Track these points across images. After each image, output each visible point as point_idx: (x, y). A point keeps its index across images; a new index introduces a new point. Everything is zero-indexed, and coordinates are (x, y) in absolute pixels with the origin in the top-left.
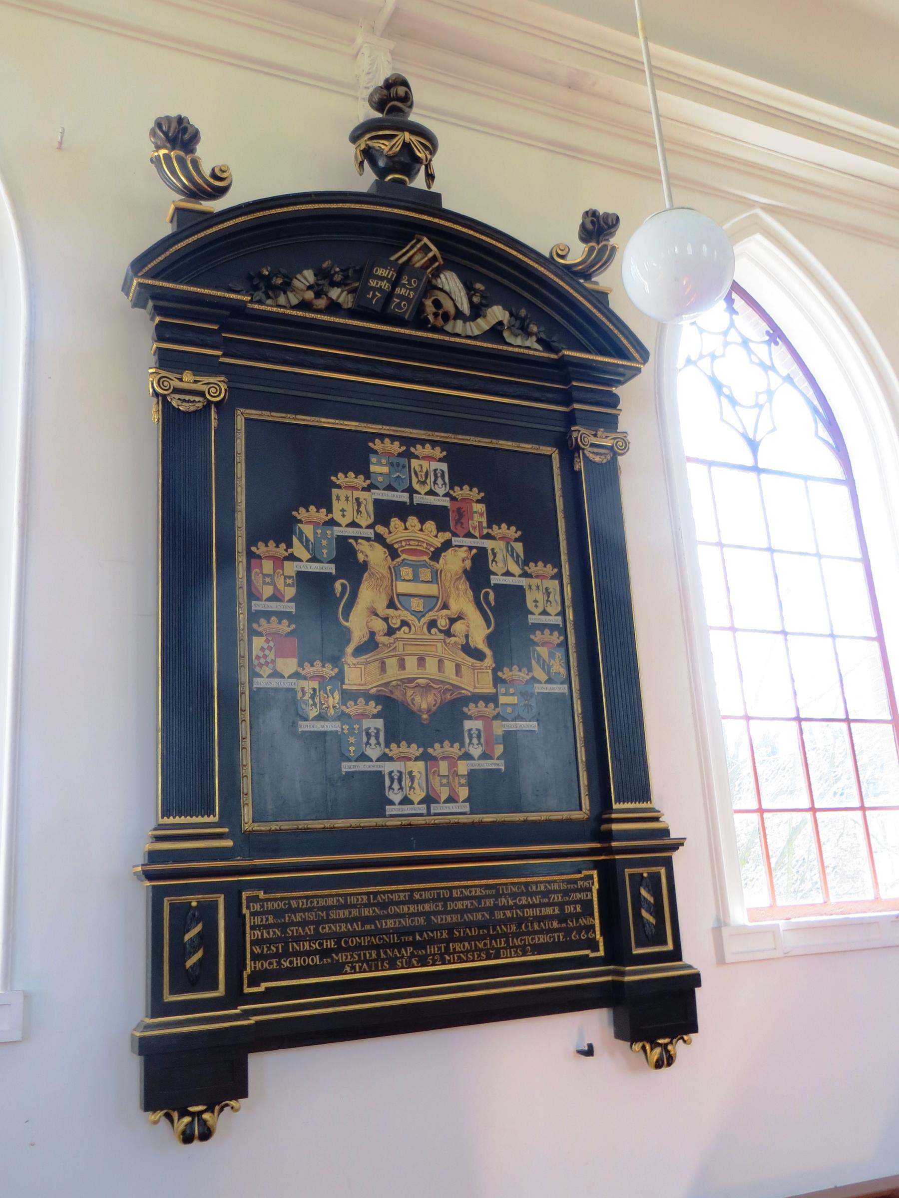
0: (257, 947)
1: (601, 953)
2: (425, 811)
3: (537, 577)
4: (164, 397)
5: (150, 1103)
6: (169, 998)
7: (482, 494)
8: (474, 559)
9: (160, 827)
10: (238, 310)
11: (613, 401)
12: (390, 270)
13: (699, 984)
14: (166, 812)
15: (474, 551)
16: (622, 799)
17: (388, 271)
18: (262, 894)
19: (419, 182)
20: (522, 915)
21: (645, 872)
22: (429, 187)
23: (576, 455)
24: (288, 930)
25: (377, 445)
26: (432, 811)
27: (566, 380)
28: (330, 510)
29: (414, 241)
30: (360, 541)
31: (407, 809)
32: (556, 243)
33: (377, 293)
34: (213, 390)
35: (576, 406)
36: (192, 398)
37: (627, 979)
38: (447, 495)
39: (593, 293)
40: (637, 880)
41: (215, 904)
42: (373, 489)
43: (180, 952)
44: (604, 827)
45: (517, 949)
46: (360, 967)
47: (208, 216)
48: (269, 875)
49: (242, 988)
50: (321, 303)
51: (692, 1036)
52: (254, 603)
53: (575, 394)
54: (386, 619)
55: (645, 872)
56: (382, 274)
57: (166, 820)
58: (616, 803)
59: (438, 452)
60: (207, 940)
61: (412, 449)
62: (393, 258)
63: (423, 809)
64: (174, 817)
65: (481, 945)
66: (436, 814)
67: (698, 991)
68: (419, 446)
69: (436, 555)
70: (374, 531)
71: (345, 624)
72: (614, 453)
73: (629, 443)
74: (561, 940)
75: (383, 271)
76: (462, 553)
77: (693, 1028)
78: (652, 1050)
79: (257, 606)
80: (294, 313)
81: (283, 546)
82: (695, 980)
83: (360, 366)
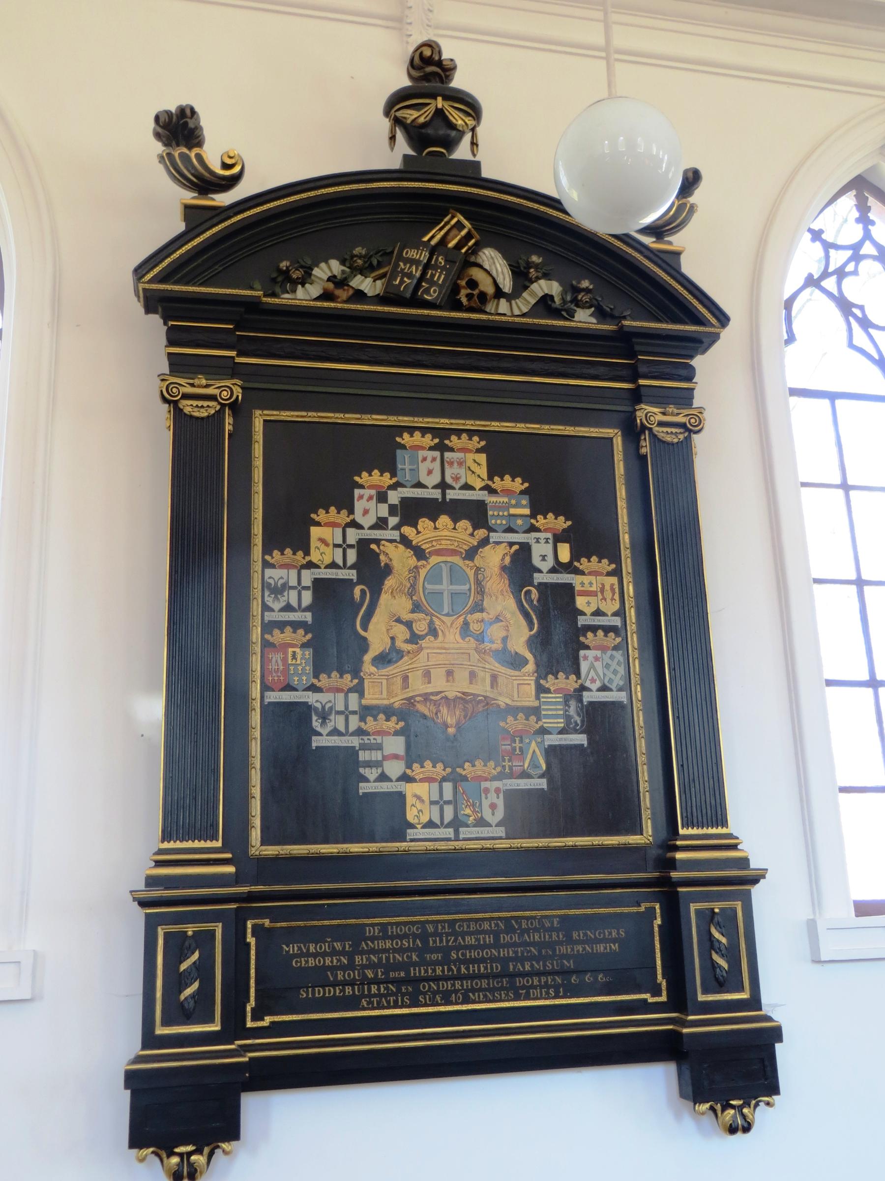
0: (369, 971)
1: (664, 998)
2: (452, 836)
3: (590, 573)
4: (176, 403)
5: (137, 1140)
6: (160, 1031)
7: (526, 485)
8: (515, 557)
9: (161, 852)
10: (253, 306)
11: (689, 375)
12: (423, 250)
13: (780, 1039)
14: (166, 836)
15: (516, 547)
16: (710, 823)
17: (420, 251)
18: (268, 922)
19: (462, 152)
20: (590, 951)
21: (717, 907)
22: (474, 155)
23: (643, 438)
24: (452, 954)
25: (406, 439)
26: (461, 836)
27: (632, 355)
28: (351, 511)
29: (450, 215)
30: (383, 542)
31: (485, 832)
32: (224, 151)
33: (405, 279)
34: (225, 393)
35: (642, 382)
36: (205, 403)
37: (685, 1031)
38: (486, 488)
39: (659, 254)
40: (709, 917)
41: (212, 933)
42: (400, 487)
43: (176, 981)
44: (669, 855)
45: (508, 992)
46: (378, 1003)
47: (218, 211)
48: (192, 907)
49: (245, 1023)
50: (343, 294)
51: (775, 1097)
52: (266, 613)
53: (642, 369)
54: (409, 624)
55: (717, 907)
56: (413, 255)
57: (166, 845)
58: (683, 829)
59: (476, 442)
60: (204, 970)
61: (447, 442)
62: (426, 239)
63: (449, 832)
64: (175, 842)
65: (536, 982)
66: (465, 840)
67: (778, 1046)
68: (454, 438)
69: (471, 554)
70: (400, 533)
71: (362, 633)
72: (690, 430)
73: (704, 420)
74: (337, 994)
75: (414, 252)
76: (502, 549)
77: (773, 1089)
78: (723, 1111)
79: (269, 616)
80: (346, 306)
81: (300, 553)
82: (776, 1034)
83: (419, 357)
